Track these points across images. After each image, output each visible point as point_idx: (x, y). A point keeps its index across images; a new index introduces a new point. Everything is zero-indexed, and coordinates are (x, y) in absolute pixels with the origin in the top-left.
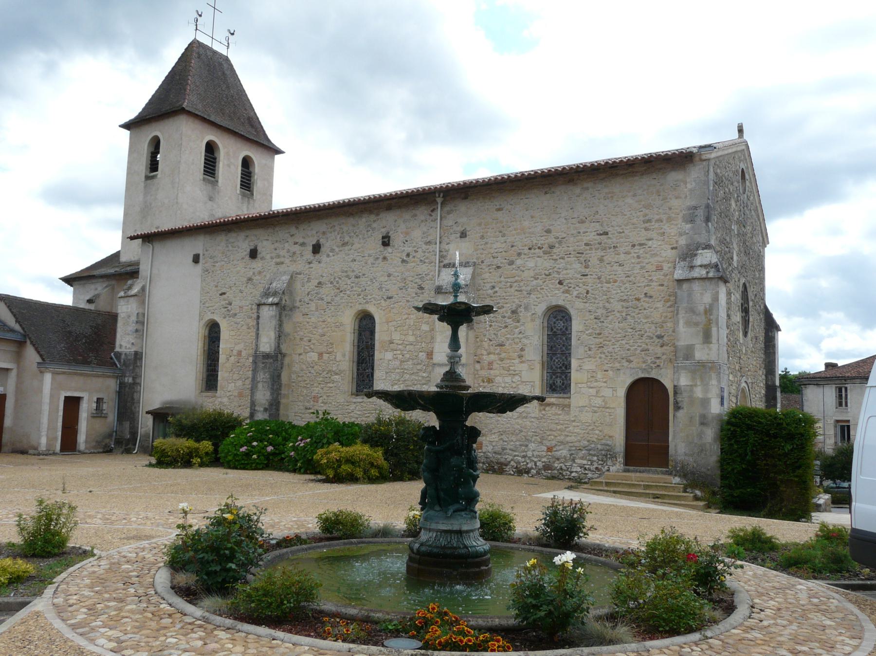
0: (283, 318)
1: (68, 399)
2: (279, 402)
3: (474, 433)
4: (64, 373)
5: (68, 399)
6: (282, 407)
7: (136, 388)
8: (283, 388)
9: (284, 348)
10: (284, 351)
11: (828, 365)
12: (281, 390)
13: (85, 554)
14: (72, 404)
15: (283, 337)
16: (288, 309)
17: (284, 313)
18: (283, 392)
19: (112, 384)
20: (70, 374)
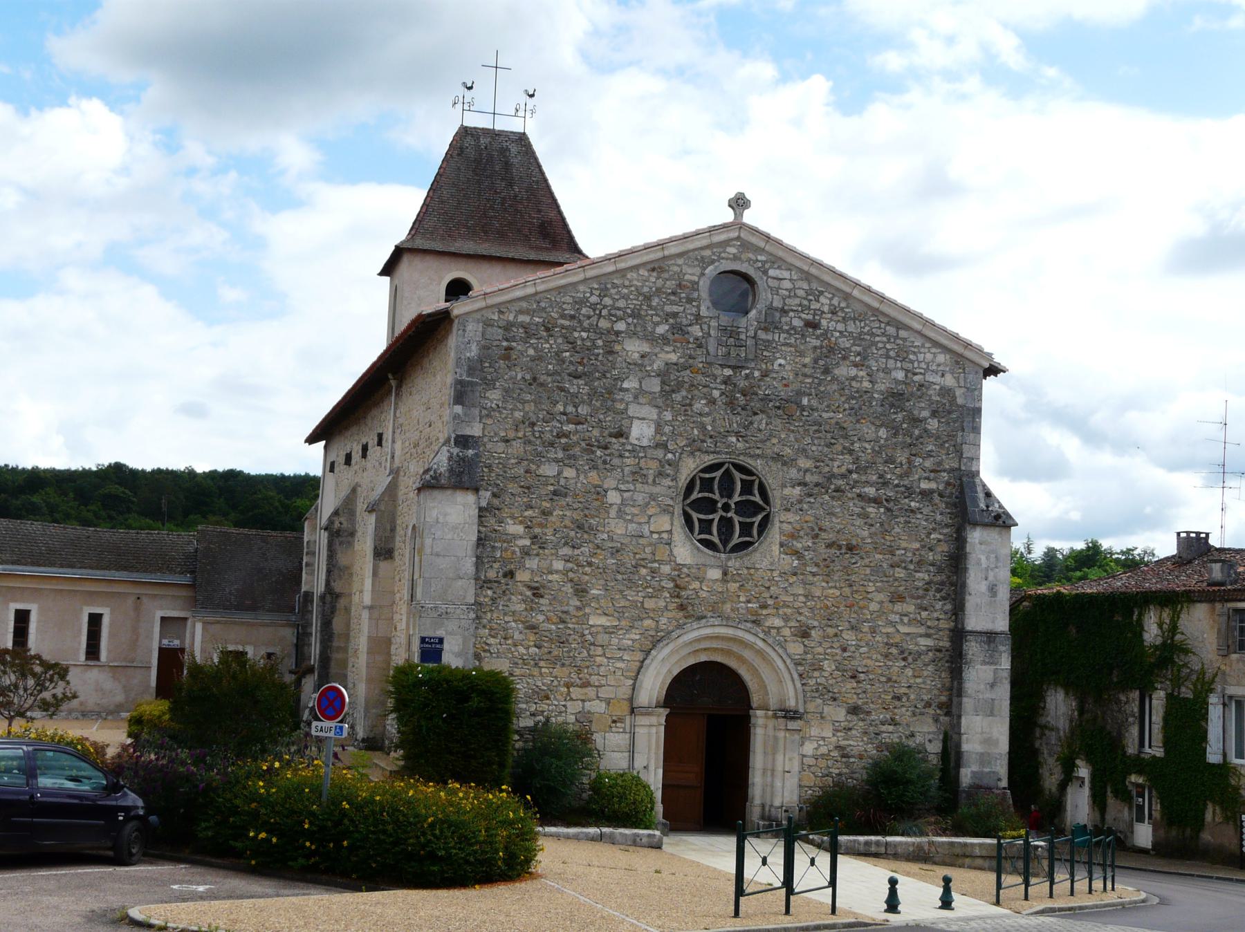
0: (337, 547)
1: (18, 612)
2: (329, 657)
3: (130, 736)
4: (218, 622)
5: (18, 612)
6: (333, 664)
7: (307, 639)
8: (336, 639)
9: (337, 586)
10: (337, 590)
11: (225, 654)
12: (331, 642)
13: (541, 876)
14: (95, 620)
15: (336, 571)
16: (346, 534)
17: (337, 541)
18: (335, 644)
19: (289, 634)
20: (226, 622)
